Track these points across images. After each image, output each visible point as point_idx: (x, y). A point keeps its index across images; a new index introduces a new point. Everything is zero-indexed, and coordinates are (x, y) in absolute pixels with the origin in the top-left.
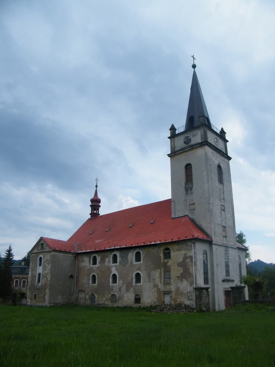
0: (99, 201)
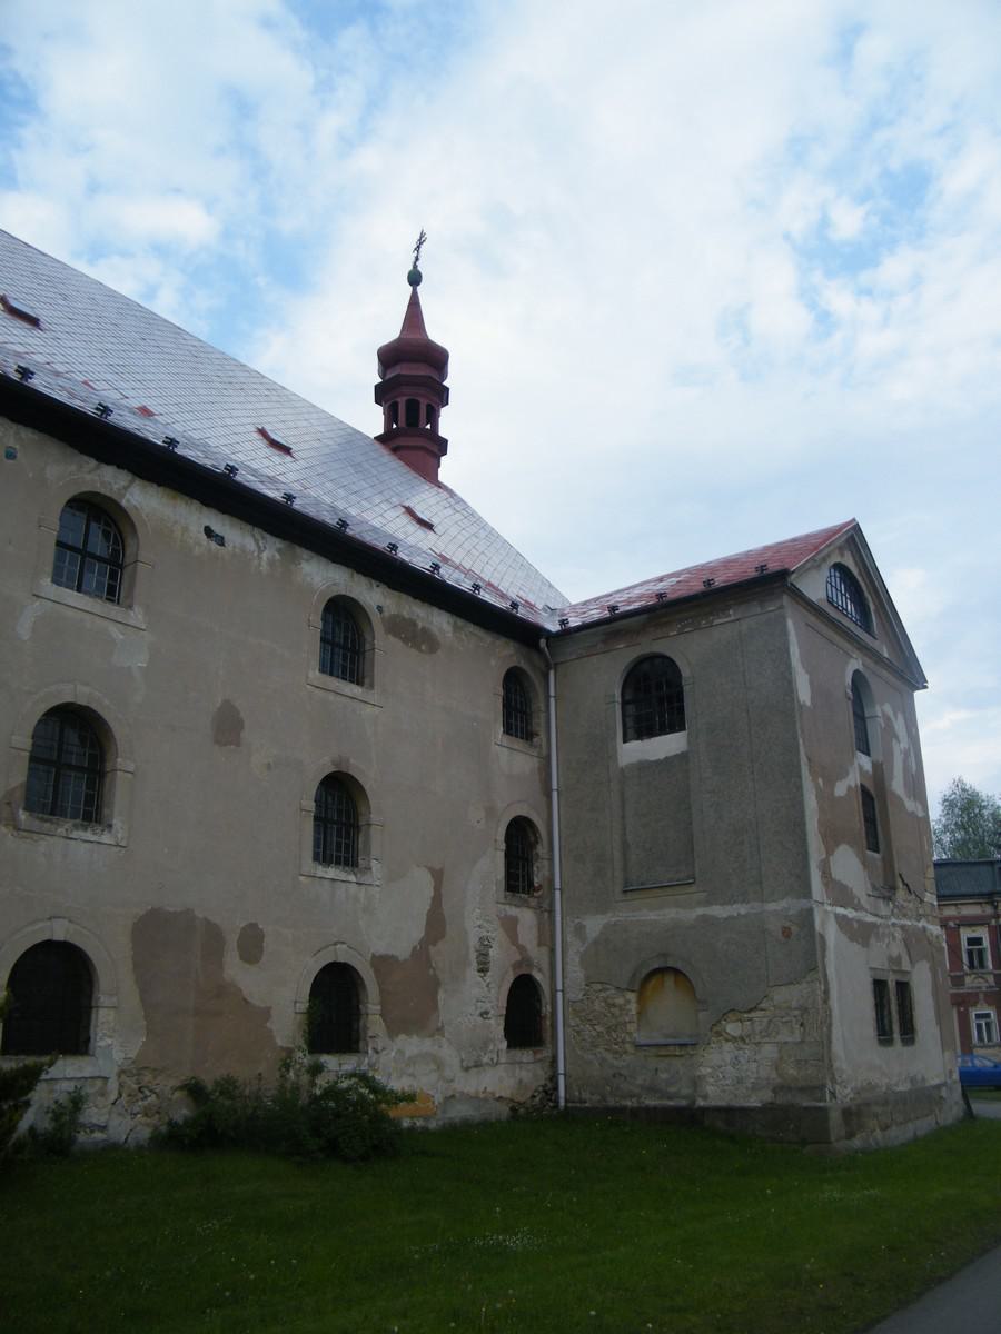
0: (436, 359)
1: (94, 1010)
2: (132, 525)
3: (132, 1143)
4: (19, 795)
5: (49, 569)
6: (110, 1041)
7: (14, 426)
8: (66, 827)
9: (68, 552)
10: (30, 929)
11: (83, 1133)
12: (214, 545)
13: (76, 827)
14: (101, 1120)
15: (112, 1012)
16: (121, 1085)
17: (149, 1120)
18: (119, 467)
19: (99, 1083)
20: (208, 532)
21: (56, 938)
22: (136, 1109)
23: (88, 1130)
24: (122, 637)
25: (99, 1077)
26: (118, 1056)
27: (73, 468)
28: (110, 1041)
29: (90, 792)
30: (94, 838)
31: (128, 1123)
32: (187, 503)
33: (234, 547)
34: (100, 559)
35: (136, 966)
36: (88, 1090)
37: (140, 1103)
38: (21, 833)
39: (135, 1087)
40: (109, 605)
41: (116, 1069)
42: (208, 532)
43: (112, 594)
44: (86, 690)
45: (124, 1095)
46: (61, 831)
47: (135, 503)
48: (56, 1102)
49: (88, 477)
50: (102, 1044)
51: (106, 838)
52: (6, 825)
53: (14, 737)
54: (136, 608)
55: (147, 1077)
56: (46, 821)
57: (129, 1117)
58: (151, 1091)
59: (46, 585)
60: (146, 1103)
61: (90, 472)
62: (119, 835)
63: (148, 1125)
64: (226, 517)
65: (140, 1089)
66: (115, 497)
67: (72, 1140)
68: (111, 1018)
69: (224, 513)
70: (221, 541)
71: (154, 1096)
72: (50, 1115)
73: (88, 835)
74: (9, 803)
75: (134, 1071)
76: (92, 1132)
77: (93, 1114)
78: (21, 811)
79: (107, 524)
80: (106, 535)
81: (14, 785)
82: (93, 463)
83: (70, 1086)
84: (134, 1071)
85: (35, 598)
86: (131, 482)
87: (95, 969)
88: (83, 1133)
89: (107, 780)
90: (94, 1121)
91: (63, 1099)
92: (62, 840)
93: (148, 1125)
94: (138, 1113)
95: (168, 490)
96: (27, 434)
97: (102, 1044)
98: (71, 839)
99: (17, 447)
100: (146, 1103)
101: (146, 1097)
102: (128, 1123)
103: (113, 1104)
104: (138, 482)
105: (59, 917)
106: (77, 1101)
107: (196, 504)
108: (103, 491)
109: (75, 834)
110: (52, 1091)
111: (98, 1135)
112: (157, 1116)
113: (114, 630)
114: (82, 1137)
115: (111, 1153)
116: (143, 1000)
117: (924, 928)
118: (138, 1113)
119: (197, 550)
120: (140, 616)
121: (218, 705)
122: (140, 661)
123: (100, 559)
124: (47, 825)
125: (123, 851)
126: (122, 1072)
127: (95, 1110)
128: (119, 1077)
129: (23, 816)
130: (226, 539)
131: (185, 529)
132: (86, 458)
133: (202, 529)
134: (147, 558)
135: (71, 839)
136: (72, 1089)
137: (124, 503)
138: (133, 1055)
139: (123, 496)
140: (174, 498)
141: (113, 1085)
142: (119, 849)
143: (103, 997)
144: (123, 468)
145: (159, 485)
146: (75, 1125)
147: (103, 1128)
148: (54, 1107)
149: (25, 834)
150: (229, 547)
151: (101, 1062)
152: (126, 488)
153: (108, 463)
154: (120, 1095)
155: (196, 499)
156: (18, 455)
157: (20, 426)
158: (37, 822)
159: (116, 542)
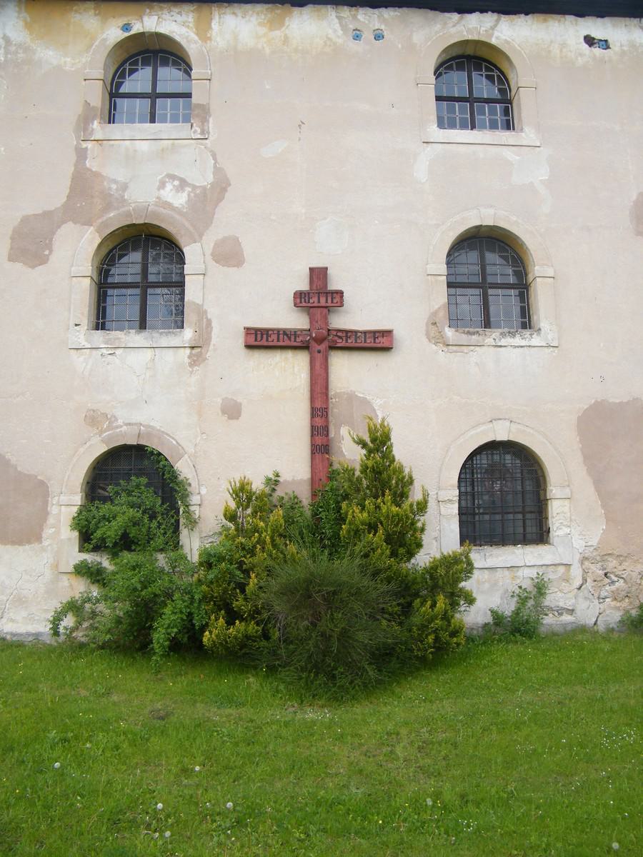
1: (549, 502)
2: (508, 58)
3: (601, 627)
4: (443, 315)
5: (434, 118)
6: (568, 530)
7: (376, 11)
8: (493, 336)
9: (456, 104)
10: (473, 432)
11: (551, 615)
12: (597, 51)
13: (503, 335)
14: (569, 604)
15: (567, 502)
16: (585, 572)
17: (618, 604)
18: (482, 12)
19: (561, 569)
20: (590, 41)
21: (499, 439)
22: (603, 594)
23: (556, 614)
24: (518, 158)
25: (559, 564)
26: (579, 544)
27: (438, 27)
28: (568, 530)
29: (522, 304)
30: (523, 343)
31: (596, 607)
32: (559, 21)
33: (621, 46)
34: (488, 101)
35: (587, 458)
36: (551, 575)
37: (608, 588)
38: (450, 347)
39: (601, 573)
40: (507, 133)
41: (578, 557)
42: (590, 41)
43: (509, 126)
44: (491, 211)
45: (588, 580)
46: (489, 341)
47: (504, 38)
48: (520, 587)
49: (453, 30)
50: (560, 533)
51: (536, 341)
52: (436, 344)
53: (428, 266)
54: (526, 129)
55: (612, 564)
56: (473, 334)
57: (596, 602)
58: (616, 576)
59: (435, 133)
60: (613, 588)
61: (454, 26)
62: (550, 337)
63: (618, 609)
64: (607, 20)
65: (606, 574)
66: (483, 39)
67: (538, 621)
68: (566, 509)
69: (602, 17)
70: (605, 44)
71: (622, 581)
72: (515, 599)
73: (517, 341)
74: (435, 324)
75: (598, 558)
76: (560, 614)
77: (555, 598)
78: (447, 329)
79: (488, 69)
80: (490, 78)
81: (436, 307)
82: (455, 16)
83: (532, 573)
84: (598, 558)
85: (425, 145)
86: (498, 21)
87: (541, 459)
88: (551, 615)
89: (532, 290)
90: (561, 604)
91: (527, 584)
92: (492, 349)
93: (618, 609)
94: (606, 598)
95: (536, 15)
96: (389, 14)
97: (560, 533)
98: (501, 346)
99: (383, 27)
100: (613, 588)
101: (613, 582)
102: (596, 607)
103: (579, 589)
104: (504, 18)
105: (500, 419)
106: (540, 588)
107: (570, 18)
108: (470, 37)
109: (503, 343)
110: (514, 578)
111: (567, 618)
112: (627, 600)
113: (508, 154)
114: (549, 620)
115: (579, 637)
116: (598, 490)
117: (96, 46)
118: (606, 598)
119: (580, 61)
120: (532, 135)
121: (634, 198)
122: (543, 173)
123: (488, 101)
124: (475, 337)
125: (556, 349)
126: (585, 559)
127: (560, 594)
128: (582, 564)
129: (449, 333)
130: (610, 41)
131: (563, 45)
132: (447, 15)
133: (582, 40)
134: (522, 78)
135: (501, 346)
136: (535, 575)
137: (494, 41)
138: (594, 542)
139: (492, 35)
140: (545, 21)
141: (576, 572)
142: (552, 349)
143: (555, 490)
144: (487, 12)
145: (527, 14)
146: (540, 610)
147: (571, 612)
148: (518, 591)
149: (454, 348)
150: (615, 47)
151: (561, 550)
152: (493, 28)
153: (470, 11)
154: (585, 581)
155: (521, 13)
156: (385, 34)
157: (381, 10)
158: (464, 336)
159: (500, 81)
